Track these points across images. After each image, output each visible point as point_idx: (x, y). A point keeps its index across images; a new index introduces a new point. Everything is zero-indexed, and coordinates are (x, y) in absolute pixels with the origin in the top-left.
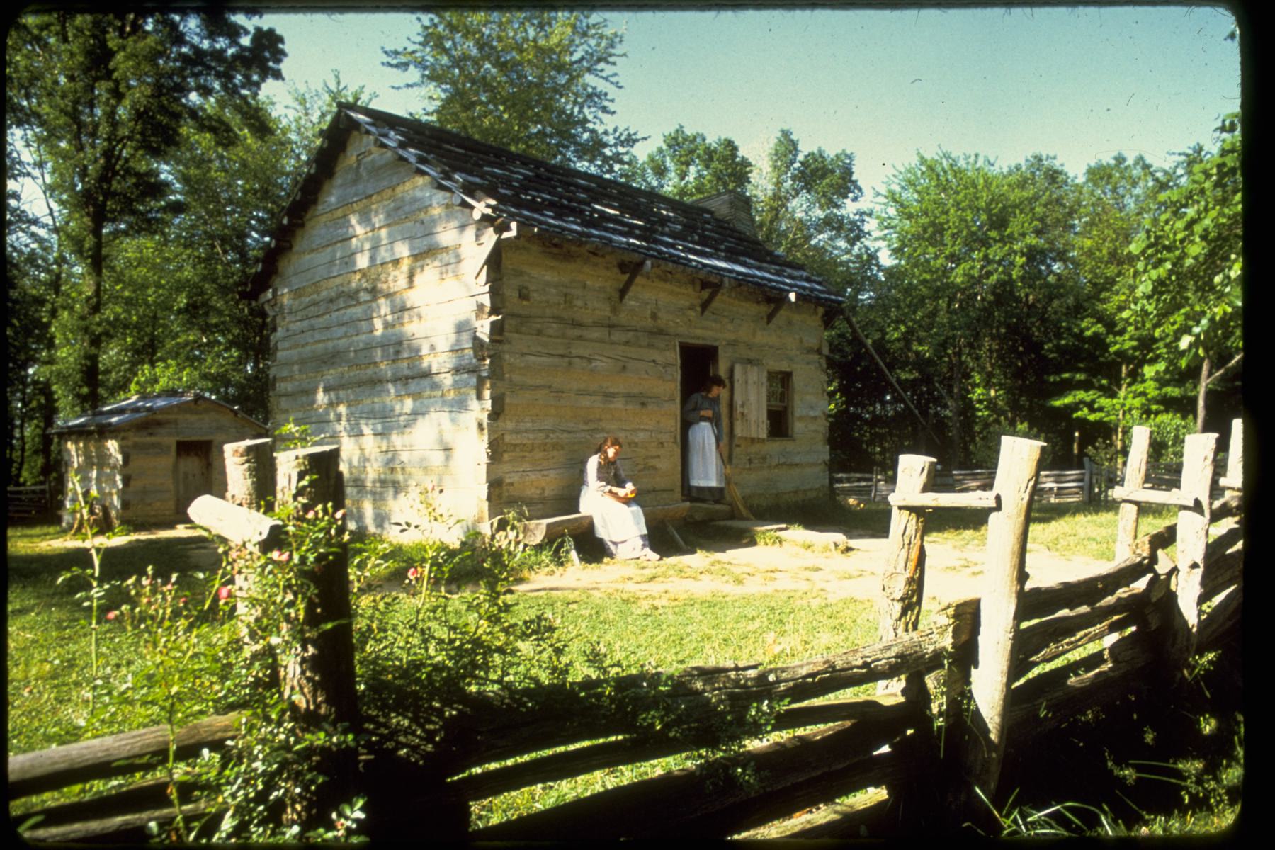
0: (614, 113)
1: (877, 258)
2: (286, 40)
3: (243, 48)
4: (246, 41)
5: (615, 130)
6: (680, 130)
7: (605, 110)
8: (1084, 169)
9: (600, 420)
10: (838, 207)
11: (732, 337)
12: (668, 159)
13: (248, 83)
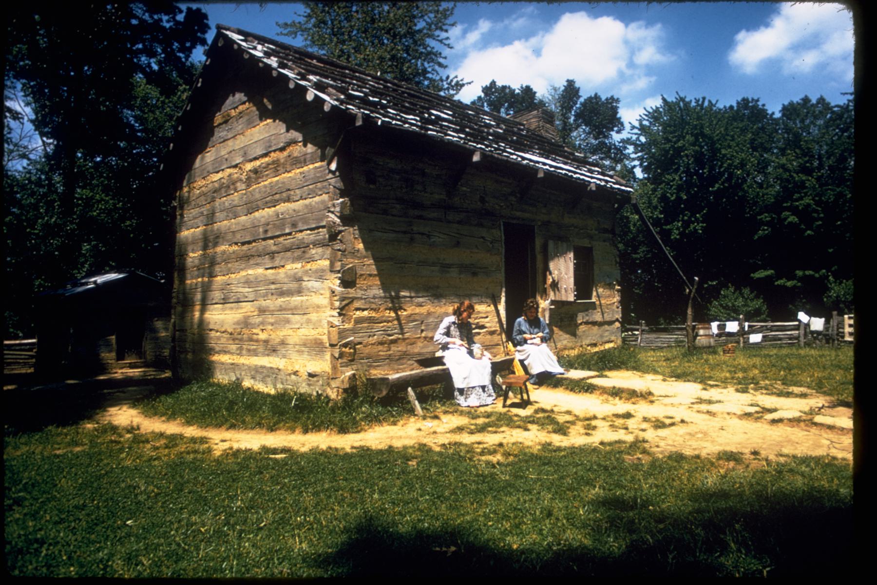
0: (446, 67)
2: (209, 17)
4: (180, 17)
8: (780, 108)
9: (438, 287)
13: (183, 49)
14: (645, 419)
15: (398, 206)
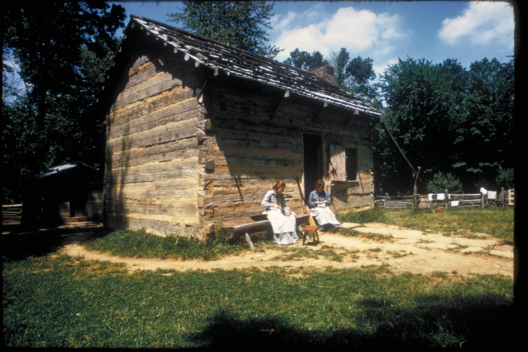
0: (269, 40)
1: (381, 104)
2: (126, 10)
3: (107, 14)
4: (109, 10)
5: (269, 47)
6: (297, 50)
7: (265, 39)
9: (264, 173)
10: (365, 82)
11: (328, 131)
12: (292, 63)
13: (110, 30)
14: (389, 252)
15: (240, 124)
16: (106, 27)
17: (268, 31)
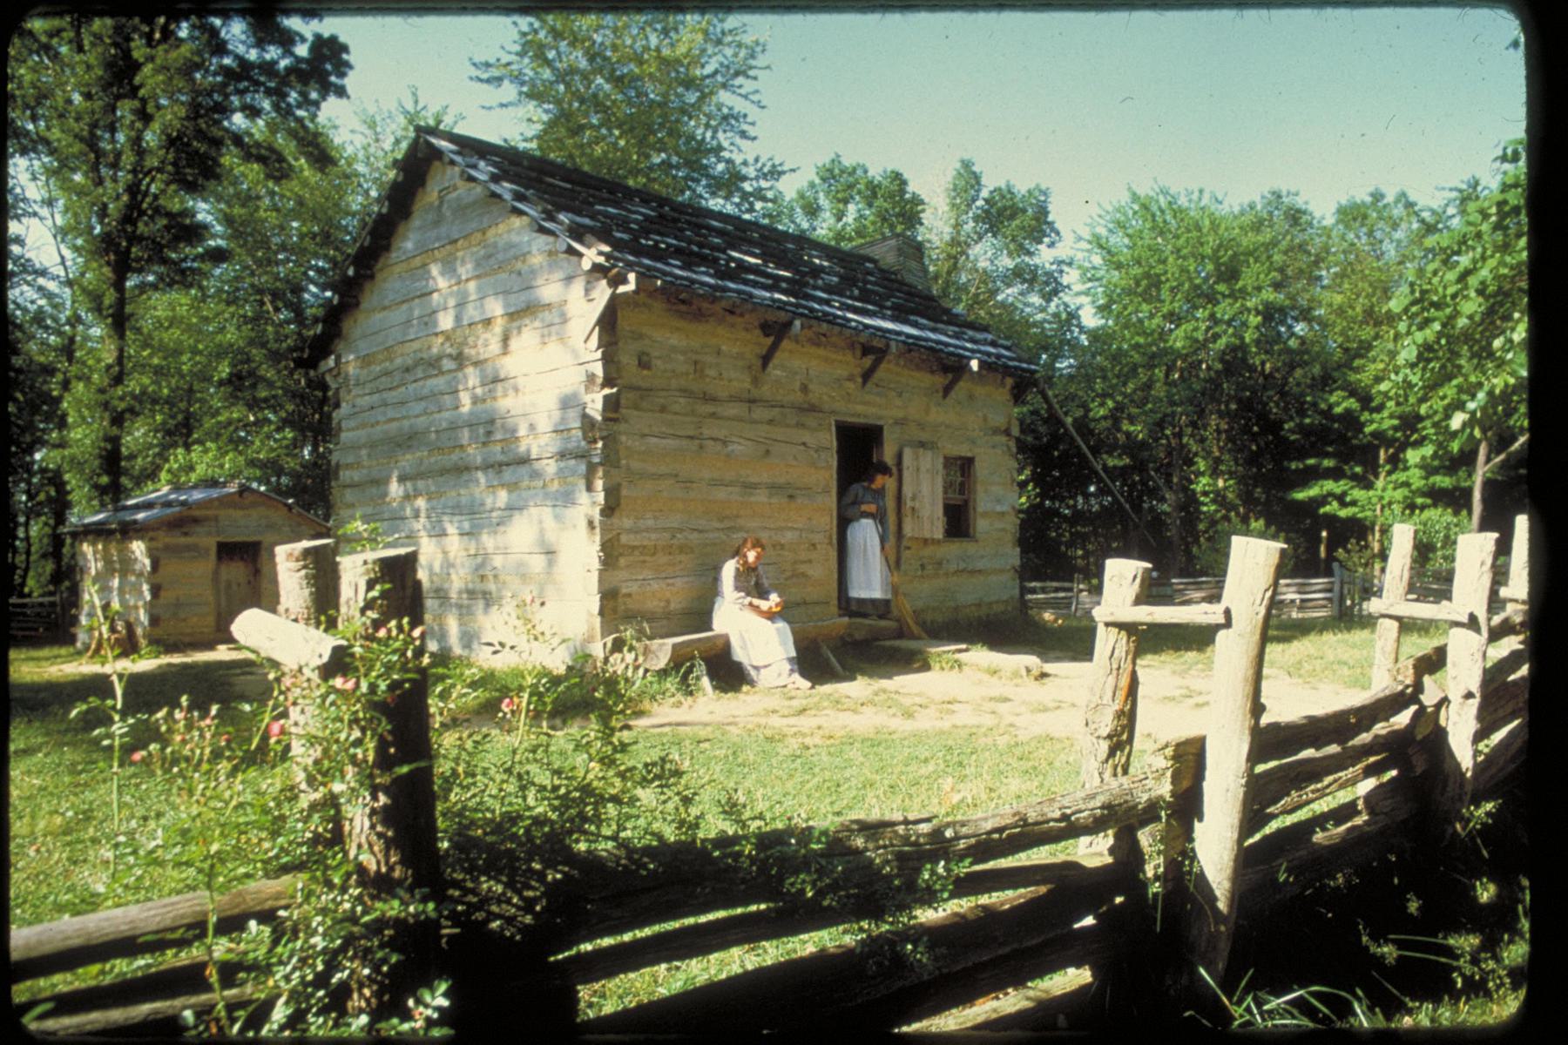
1: (1078, 318)
2: (352, 49)
3: (299, 60)
4: (302, 50)
7: (743, 134)
8: (1333, 208)
9: (737, 516)
14: (1024, 702)
15: (681, 400)
16: (294, 95)
17: (753, 112)
